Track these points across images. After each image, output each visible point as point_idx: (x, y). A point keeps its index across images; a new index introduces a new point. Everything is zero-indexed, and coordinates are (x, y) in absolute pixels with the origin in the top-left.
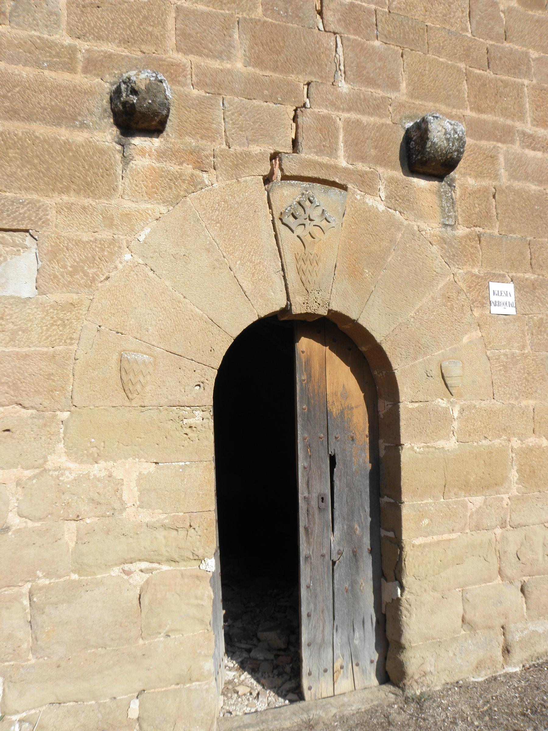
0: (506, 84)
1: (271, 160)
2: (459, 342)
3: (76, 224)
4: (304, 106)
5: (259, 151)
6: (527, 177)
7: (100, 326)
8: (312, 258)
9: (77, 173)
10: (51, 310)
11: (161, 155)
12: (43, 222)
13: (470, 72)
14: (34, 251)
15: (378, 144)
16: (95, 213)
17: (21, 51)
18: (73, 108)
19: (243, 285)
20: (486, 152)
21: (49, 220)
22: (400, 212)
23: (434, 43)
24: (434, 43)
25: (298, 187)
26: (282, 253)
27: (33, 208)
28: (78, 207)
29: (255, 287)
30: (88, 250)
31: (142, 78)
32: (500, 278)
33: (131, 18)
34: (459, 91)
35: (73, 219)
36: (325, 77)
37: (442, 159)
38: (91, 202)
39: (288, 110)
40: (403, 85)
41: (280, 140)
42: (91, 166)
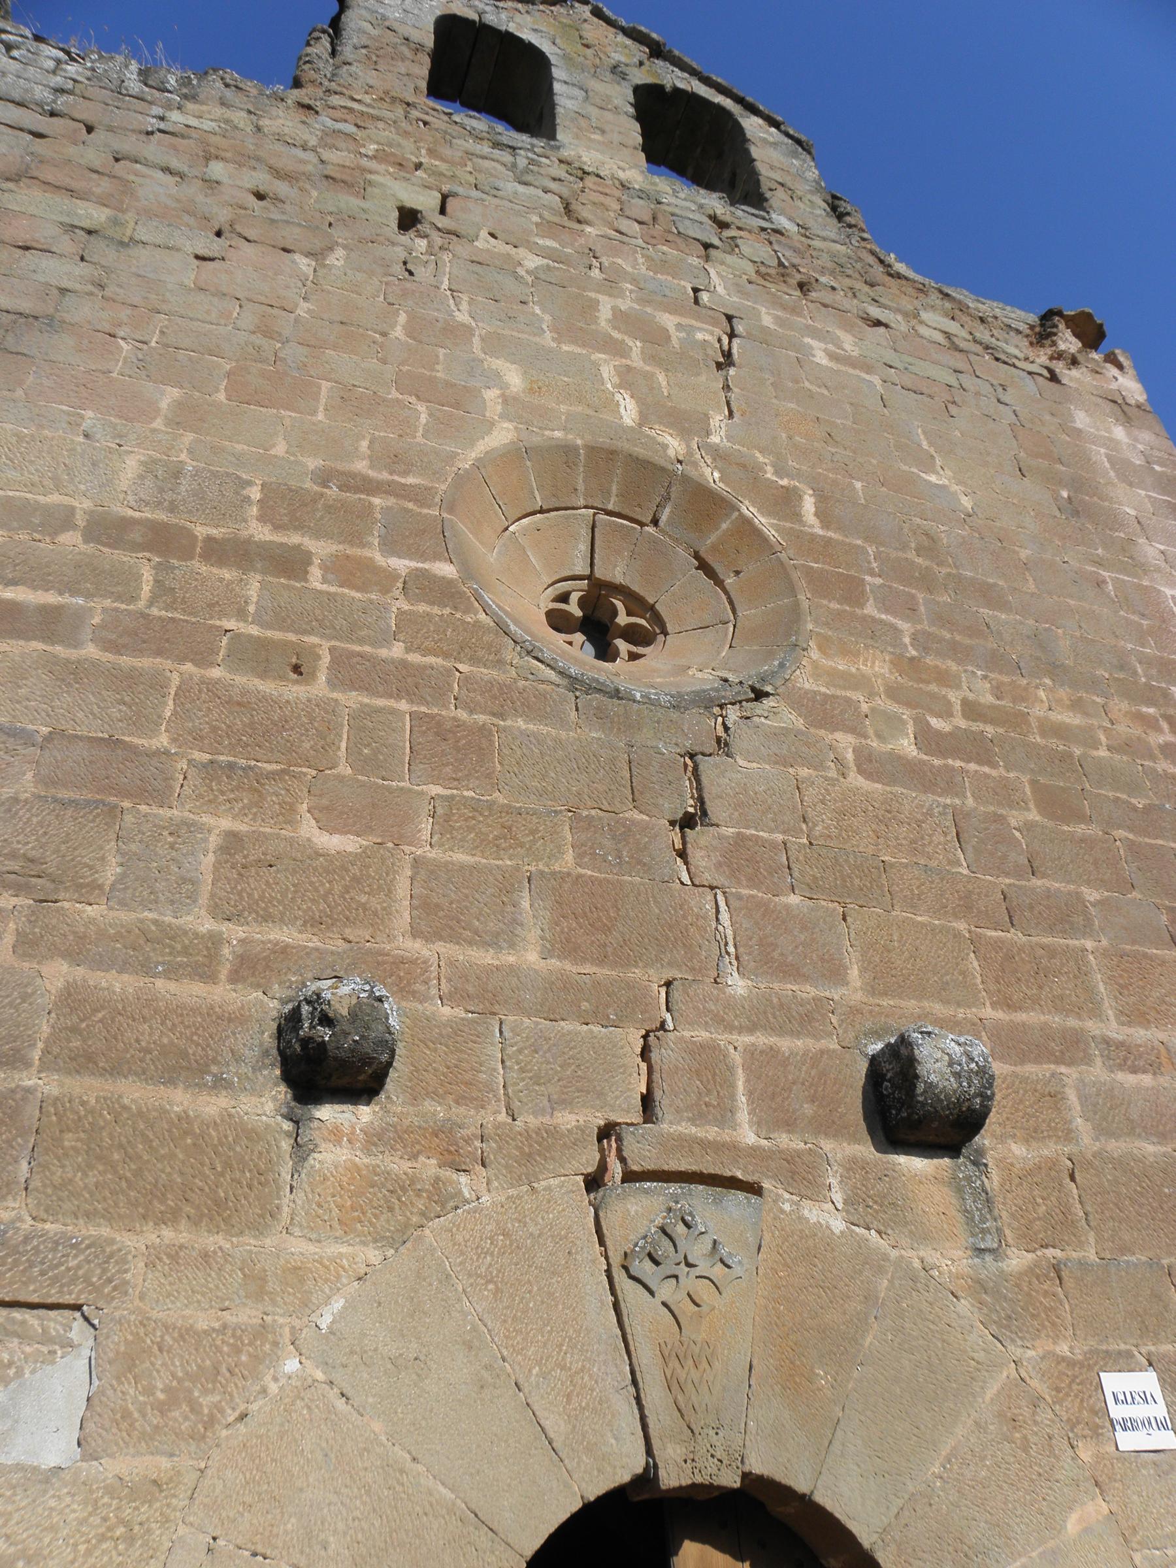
0: (1052, 952)
1: (600, 1140)
2: (1059, 1532)
3: (186, 1291)
4: (662, 1026)
5: (574, 1123)
6: (1132, 1129)
7: (214, 1539)
8: (697, 1350)
9: (197, 1181)
10: (106, 1500)
11: (374, 1139)
12: (115, 1289)
13: (979, 936)
14: (86, 1353)
15: (816, 1091)
16: (228, 1267)
17: (118, 945)
18: (203, 1049)
19: (546, 1424)
20: (1039, 1087)
21: (127, 1283)
22: (879, 1232)
23: (902, 890)
24: (902, 890)
25: (659, 1194)
26: (631, 1343)
27: (96, 1257)
28: (194, 1254)
29: (574, 1427)
30: (205, 1351)
31: (342, 995)
32: (1124, 1362)
33: (329, 882)
34: (963, 973)
35: (180, 1280)
36: (700, 970)
37: (951, 1114)
38: (222, 1243)
39: (631, 1038)
40: (854, 973)
41: (617, 1098)
42: (227, 1165)
